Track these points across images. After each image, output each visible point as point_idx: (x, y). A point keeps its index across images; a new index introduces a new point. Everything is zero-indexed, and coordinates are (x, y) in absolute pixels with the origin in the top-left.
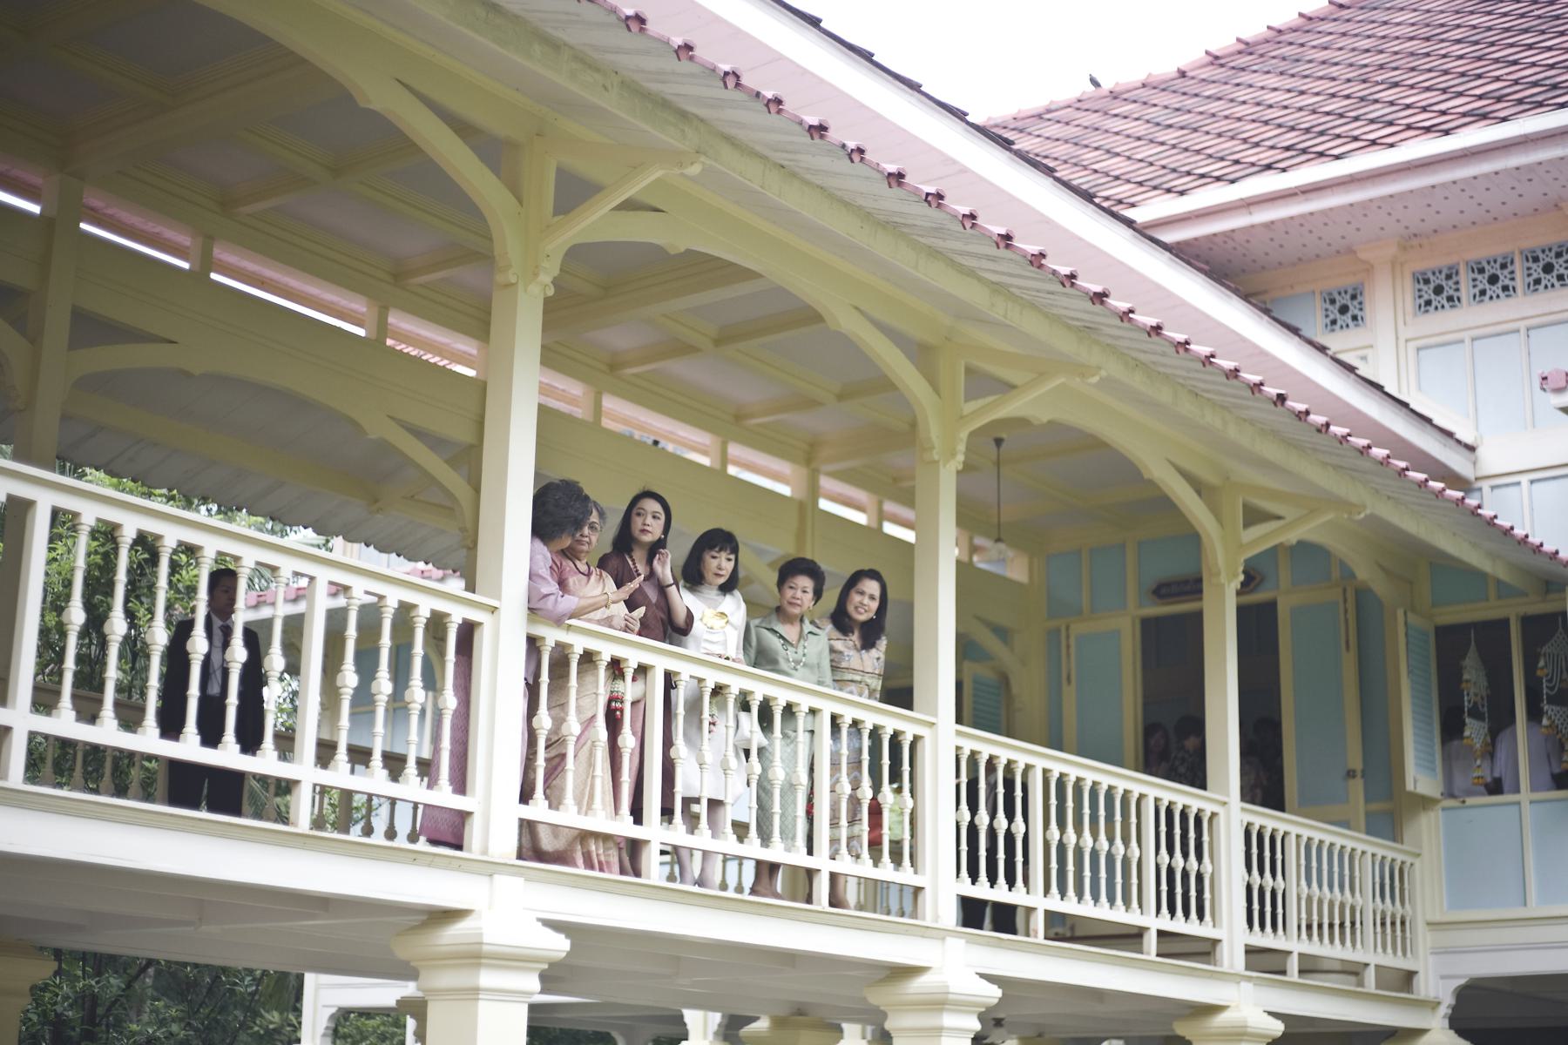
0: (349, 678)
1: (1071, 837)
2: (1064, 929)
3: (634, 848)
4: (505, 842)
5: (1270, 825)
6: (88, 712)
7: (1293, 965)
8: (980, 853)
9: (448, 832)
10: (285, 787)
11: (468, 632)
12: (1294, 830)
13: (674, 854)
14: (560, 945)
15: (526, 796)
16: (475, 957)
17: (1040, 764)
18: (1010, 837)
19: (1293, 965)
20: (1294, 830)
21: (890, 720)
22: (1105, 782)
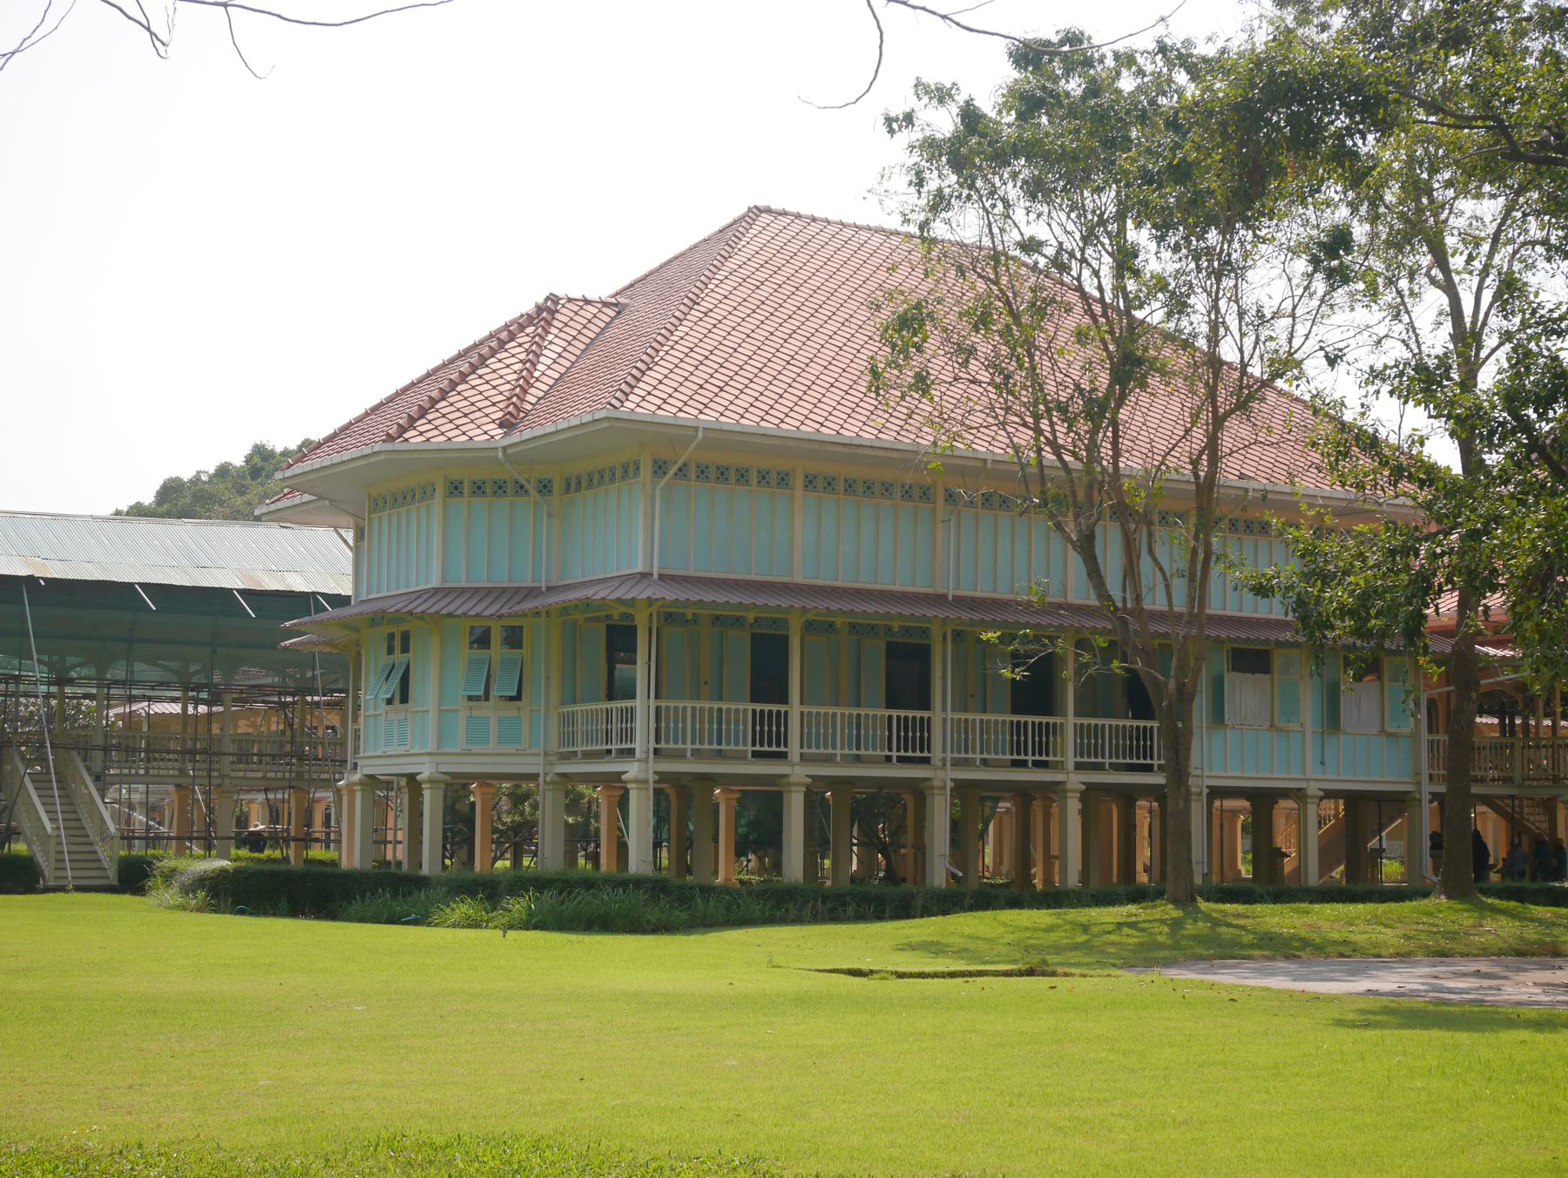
6: (770, 745)
12: (733, 707)
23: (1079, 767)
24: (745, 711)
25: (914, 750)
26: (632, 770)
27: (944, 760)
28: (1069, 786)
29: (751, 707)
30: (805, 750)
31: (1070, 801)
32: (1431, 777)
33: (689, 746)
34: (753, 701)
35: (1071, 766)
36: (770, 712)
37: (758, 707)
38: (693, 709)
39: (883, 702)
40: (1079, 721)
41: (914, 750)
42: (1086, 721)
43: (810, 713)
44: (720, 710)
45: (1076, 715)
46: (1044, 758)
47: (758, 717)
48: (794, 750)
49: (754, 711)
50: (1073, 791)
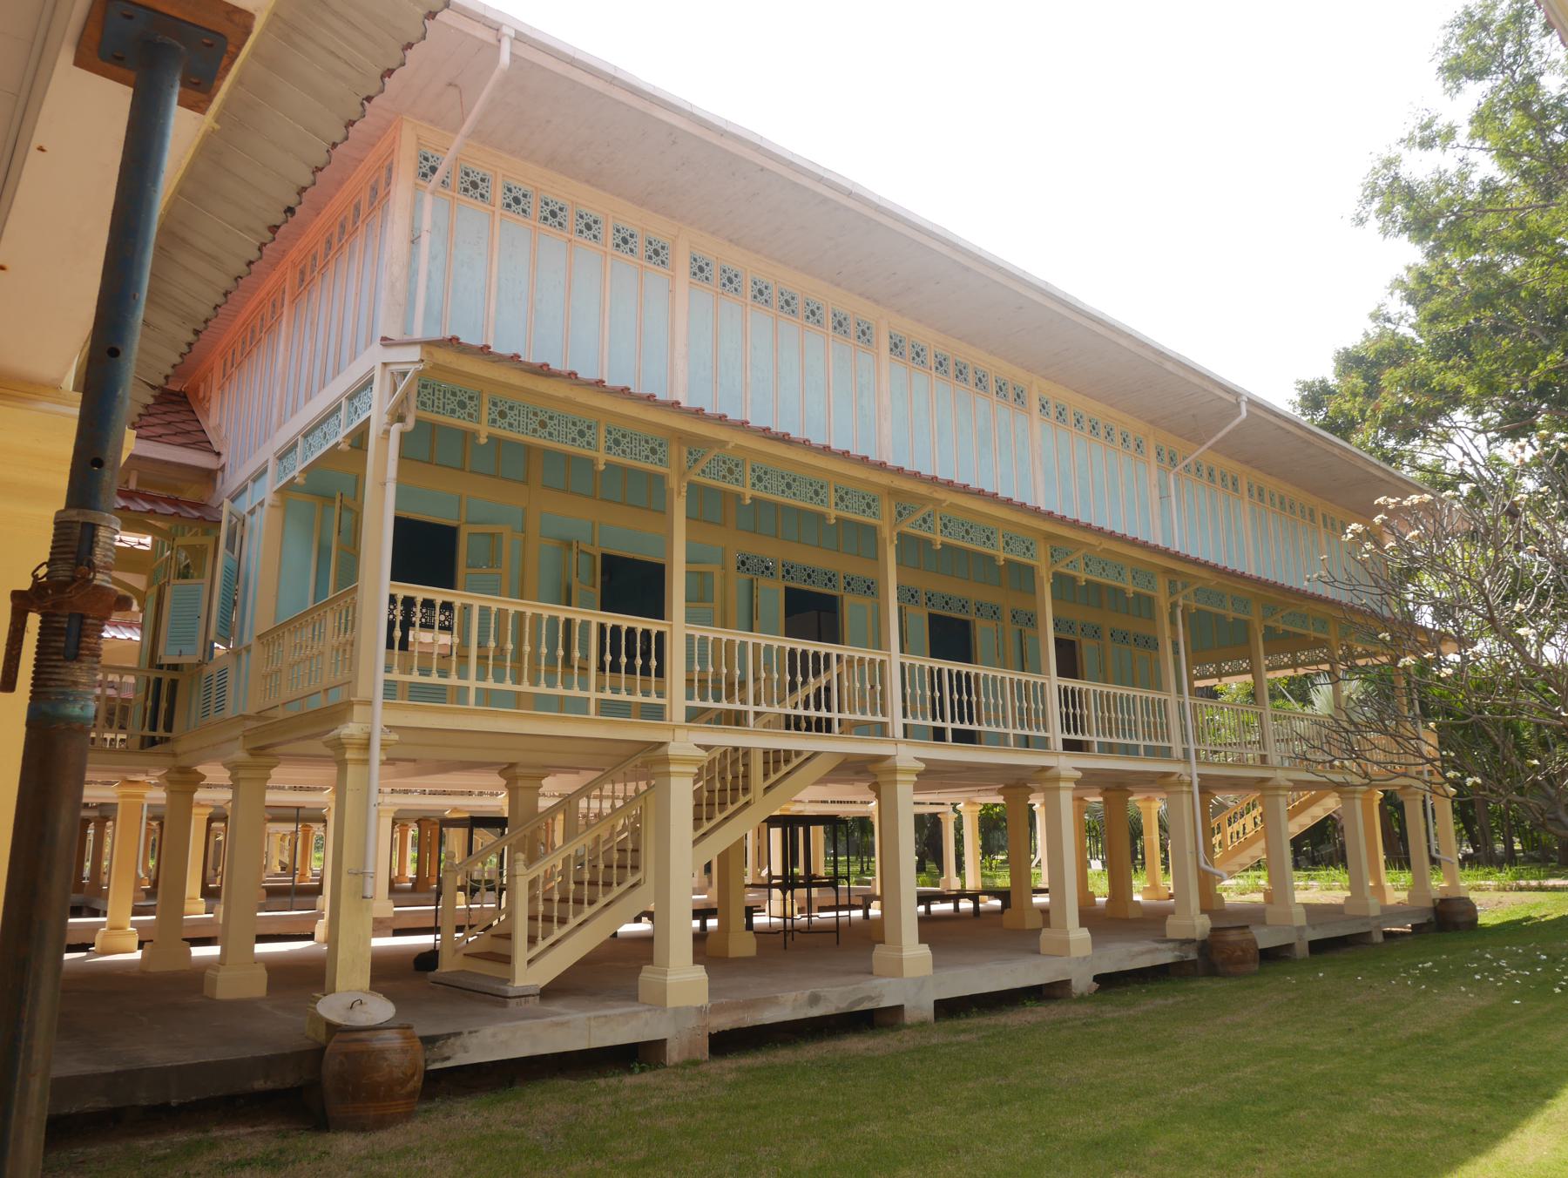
0: (956, 696)
1: (1071, 710)
2: (1108, 749)
3: (829, 721)
4: (899, 733)
5: (1157, 697)
6: (518, 680)
7: (1142, 750)
8: (1070, 722)
9: (657, 713)
10: (1137, 746)
11: (660, 635)
12: (1092, 688)
13: (757, 714)
14: (1079, 774)
15: (905, 716)
16: (1278, 788)
17: (1008, 676)
18: (1037, 711)
19: (1142, 750)
20: (1092, 688)
21: (1070, 683)
22: (1119, 692)
23: (693, 715)
24: (585, 625)
25: (535, 682)
26: (688, 744)
27: (1186, 752)
28: (673, 750)
29: (599, 618)
30: (910, 721)
31: (675, 783)
32: (390, 689)
33: (472, 683)
34: (605, 607)
35: (678, 713)
36: (520, 616)
37: (611, 619)
38: (484, 611)
39: (783, 631)
40: (698, 632)
41: (535, 682)
42: (711, 633)
43: (501, 613)
44: (568, 622)
45: (690, 618)
46: (1079, 737)
47: (612, 639)
48: (677, 700)
49: (602, 627)
50: (907, 771)
